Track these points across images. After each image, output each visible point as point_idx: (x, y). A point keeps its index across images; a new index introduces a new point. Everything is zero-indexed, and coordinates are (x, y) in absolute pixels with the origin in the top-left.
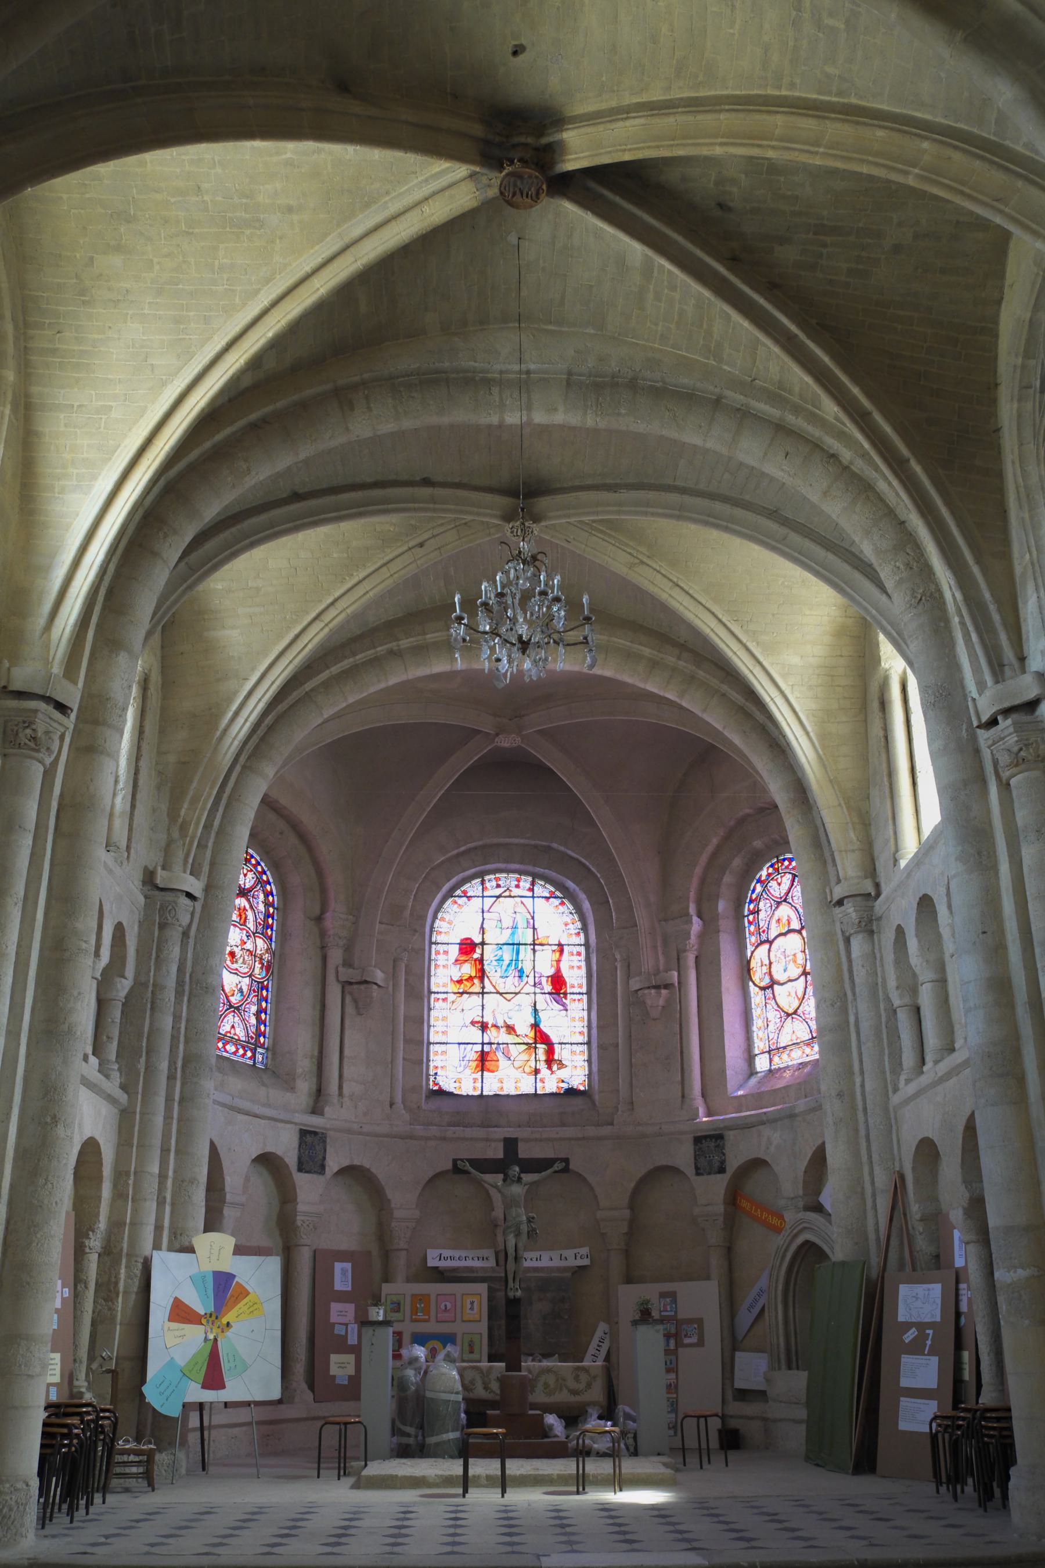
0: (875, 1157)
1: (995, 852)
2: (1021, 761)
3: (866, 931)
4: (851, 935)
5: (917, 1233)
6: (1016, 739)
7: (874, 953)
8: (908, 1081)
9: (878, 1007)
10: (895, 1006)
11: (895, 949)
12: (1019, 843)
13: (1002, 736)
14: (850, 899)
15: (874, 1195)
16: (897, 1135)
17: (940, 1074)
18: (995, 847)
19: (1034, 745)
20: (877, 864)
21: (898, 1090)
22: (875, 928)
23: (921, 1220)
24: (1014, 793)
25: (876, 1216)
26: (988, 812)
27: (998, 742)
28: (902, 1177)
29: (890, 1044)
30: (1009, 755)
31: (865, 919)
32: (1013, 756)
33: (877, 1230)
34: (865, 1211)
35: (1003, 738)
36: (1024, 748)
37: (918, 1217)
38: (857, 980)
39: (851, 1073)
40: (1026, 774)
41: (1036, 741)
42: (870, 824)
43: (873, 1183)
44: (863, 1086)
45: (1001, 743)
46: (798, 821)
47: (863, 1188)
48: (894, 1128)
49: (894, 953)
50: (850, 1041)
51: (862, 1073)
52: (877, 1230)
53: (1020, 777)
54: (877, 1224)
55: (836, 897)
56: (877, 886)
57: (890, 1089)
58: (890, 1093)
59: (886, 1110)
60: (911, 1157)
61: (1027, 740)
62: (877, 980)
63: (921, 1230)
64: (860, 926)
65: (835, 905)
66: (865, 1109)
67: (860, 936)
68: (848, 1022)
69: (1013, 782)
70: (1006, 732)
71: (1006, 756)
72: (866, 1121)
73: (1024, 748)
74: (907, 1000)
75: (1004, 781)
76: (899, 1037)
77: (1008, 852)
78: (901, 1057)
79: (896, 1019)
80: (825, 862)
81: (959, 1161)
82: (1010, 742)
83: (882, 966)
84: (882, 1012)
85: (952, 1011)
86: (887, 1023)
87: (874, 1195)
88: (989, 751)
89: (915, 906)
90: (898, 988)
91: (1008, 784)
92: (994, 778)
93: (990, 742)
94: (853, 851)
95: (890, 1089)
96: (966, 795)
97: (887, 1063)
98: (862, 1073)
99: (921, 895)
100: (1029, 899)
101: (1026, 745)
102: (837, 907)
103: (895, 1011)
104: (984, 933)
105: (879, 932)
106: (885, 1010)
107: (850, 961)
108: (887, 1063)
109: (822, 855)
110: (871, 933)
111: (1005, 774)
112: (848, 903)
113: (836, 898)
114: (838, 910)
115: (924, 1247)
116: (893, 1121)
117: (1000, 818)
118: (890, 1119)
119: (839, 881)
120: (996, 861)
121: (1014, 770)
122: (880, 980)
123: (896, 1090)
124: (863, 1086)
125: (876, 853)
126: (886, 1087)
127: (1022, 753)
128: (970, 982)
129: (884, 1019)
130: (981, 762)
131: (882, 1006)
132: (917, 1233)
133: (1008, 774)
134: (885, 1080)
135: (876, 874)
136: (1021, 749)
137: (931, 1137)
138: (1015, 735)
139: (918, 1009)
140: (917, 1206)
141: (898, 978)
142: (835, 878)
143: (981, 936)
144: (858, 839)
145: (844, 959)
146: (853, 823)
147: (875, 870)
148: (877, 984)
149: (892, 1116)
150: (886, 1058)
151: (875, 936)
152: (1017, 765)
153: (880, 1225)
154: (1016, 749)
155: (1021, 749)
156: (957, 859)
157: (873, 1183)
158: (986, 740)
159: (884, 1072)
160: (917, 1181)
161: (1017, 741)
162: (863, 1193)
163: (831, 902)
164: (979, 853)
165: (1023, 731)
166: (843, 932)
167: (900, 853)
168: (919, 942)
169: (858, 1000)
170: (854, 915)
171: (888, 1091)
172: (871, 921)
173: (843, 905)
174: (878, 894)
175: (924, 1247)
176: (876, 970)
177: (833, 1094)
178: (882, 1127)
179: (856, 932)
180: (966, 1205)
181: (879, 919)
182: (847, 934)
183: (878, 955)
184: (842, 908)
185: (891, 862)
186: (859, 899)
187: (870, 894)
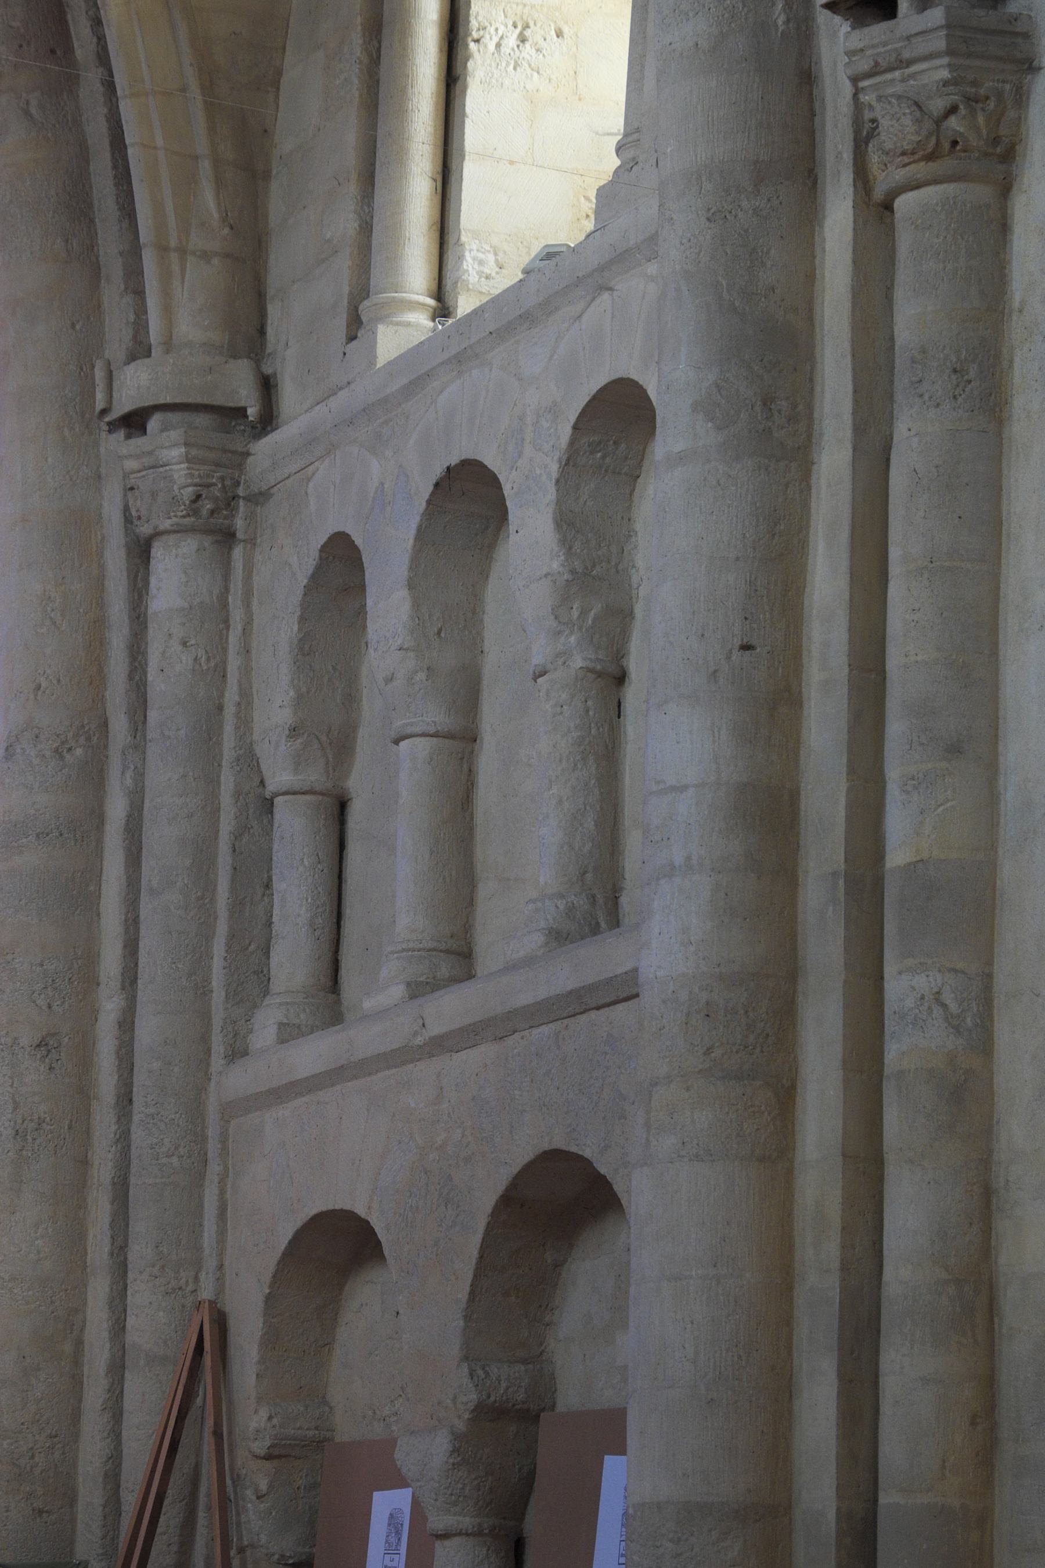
0: (139, 1252)
1: (810, 408)
2: (947, 146)
3: (209, 531)
4: (158, 534)
5: (249, 1493)
6: (945, 74)
7: (224, 605)
8: (288, 1033)
9: (212, 781)
10: (271, 787)
11: (305, 605)
12: (890, 396)
13: (906, 55)
14: (173, 417)
15: (117, 1369)
16: (222, 1192)
17: (436, 1029)
18: (812, 390)
19: (992, 104)
20: (273, 311)
21: (245, 1053)
22: (239, 523)
23: (268, 1457)
24: (905, 240)
25: (116, 1434)
26: (810, 278)
27: (890, 69)
28: (221, 1322)
29: (237, 906)
30: (918, 121)
31: (216, 492)
32: (928, 125)
33: (113, 1477)
34: (76, 1416)
35: (909, 63)
36: (963, 110)
37: (260, 1447)
38: (157, 685)
39: (90, 980)
40: (950, 189)
41: (1000, 95)
42: (267, 175)
43: (119, 1328)
44: (127, 1024)
45: (897, 74)
46: (27, 113)
47: (79, 1343)
48: (214, 1168)
49: (302, 620)
50: (98, 875)
51: (130, 979)
52: (113, 1477)
53: (931, 193)
54: (115, 1459)
55: (125, 402)
56: (267, 386)
57: (218, 1046)
58: (217, 1062)
59: (196, 1111)
60: (270, 1261)
61: (974, 83)
62: (222, 696)
63: (263, 1486)
64: (195, 512)
65: (113, 427)
66: (125, 1100)
67: (189, 545)
68: (99, 818)
69: (904, 203)
70: (922, 47)
71: (907, 121)
72: (124, 1139)
73: (963, 110)
74: (314, 776)
75: (879, 193)
76: (268, 885)
77: (855, 413)
78: (267, 952)
79: (268, 831)
80: (95, 273)
81: (463, 1293)
82: (925, 79)
83: (246, 651)
84: (226, 799)
85: (479, 834)
86: (237, 836)
87: (117, 1369)
88: (848, 88)
89: (426, 490)
90: (294, 732)
91: (887, 206)
92: (847, 177)
93: (864, 65)
94: (205, 256)
95: (218, 1046)
96: (756, 211)
97: (217, 964)
98: (130, 979)
99: (454, 461)
100: (895, 569)
101: (972, 100)
102: (121, 434)
103: (267, 806)
104: (746, 647)
105: (252, 542)
106: (237, 794)
107: (139, 618)
108: (217, 964)
109: (91, 247)
110: (227, 537)
111: (883, 180)
112: (165, 429)
113: (124, 403)
114: (116, 443)
115: (263, 1539)
116: (213, 1147)
117: (847, 305)
118: (204, 1139)
119: (140, 350)
120: (810, 436)
121: (921, 169)
122: (231, 696)
123: (237, 1052)
124: (127, 1024)
125: (274, 281)
126: (205, 1039)
127: (953, 122)
128: (684, 788)
129: (226, 825)
130: (813, 114)
131: (228, 781)
132: (249, 1493)
133: (899, 175)
134: (205, 1016)
135: (263, 345)
136: (953, 110)
137: (361, 1211)
138: (946, 60)
139: (342, 806)
140: (264, 1413)
141: (300, 701)
142: (127, 334)
143: (736, 656)
144: (224, 219)
145: (117, 608)
146: (217, 162)
147: (262, 331)
148: (220, 708)
149: (212, 1132)
150: (219, 947)
151: (238, 552)
152: (931, 157)
153: (126, 1465)
154: (938, 105)
155: (953, 110)
156: (695, 407)
157: (119, 1328)
158: (850, 54)
159: (203, 992)
160: (270, 1340)
161: (946, 83)
162: (77, 1359)
163: (104, 412)
164: (767, 402)
165: (970, 55)
166: (128, 519)
167: (374, 299)
168: (416, 605)
169: (153, 751)
170: (180, 472)
171: (208, 1052)
172: (230, 501)
173: (143, 430)
174: (268, 421)
175: (263, 1539)
176: (224, 662)
177: (25, 1041)
178: (175, 1160)
179: (179, 530)
180: (461, 1426)
181: (259, 498)
182: (145, 530)
183: (237, 616)
184: (139, 443)
185: (341, 322)
186: (202, 420)
187: (241, 412)
